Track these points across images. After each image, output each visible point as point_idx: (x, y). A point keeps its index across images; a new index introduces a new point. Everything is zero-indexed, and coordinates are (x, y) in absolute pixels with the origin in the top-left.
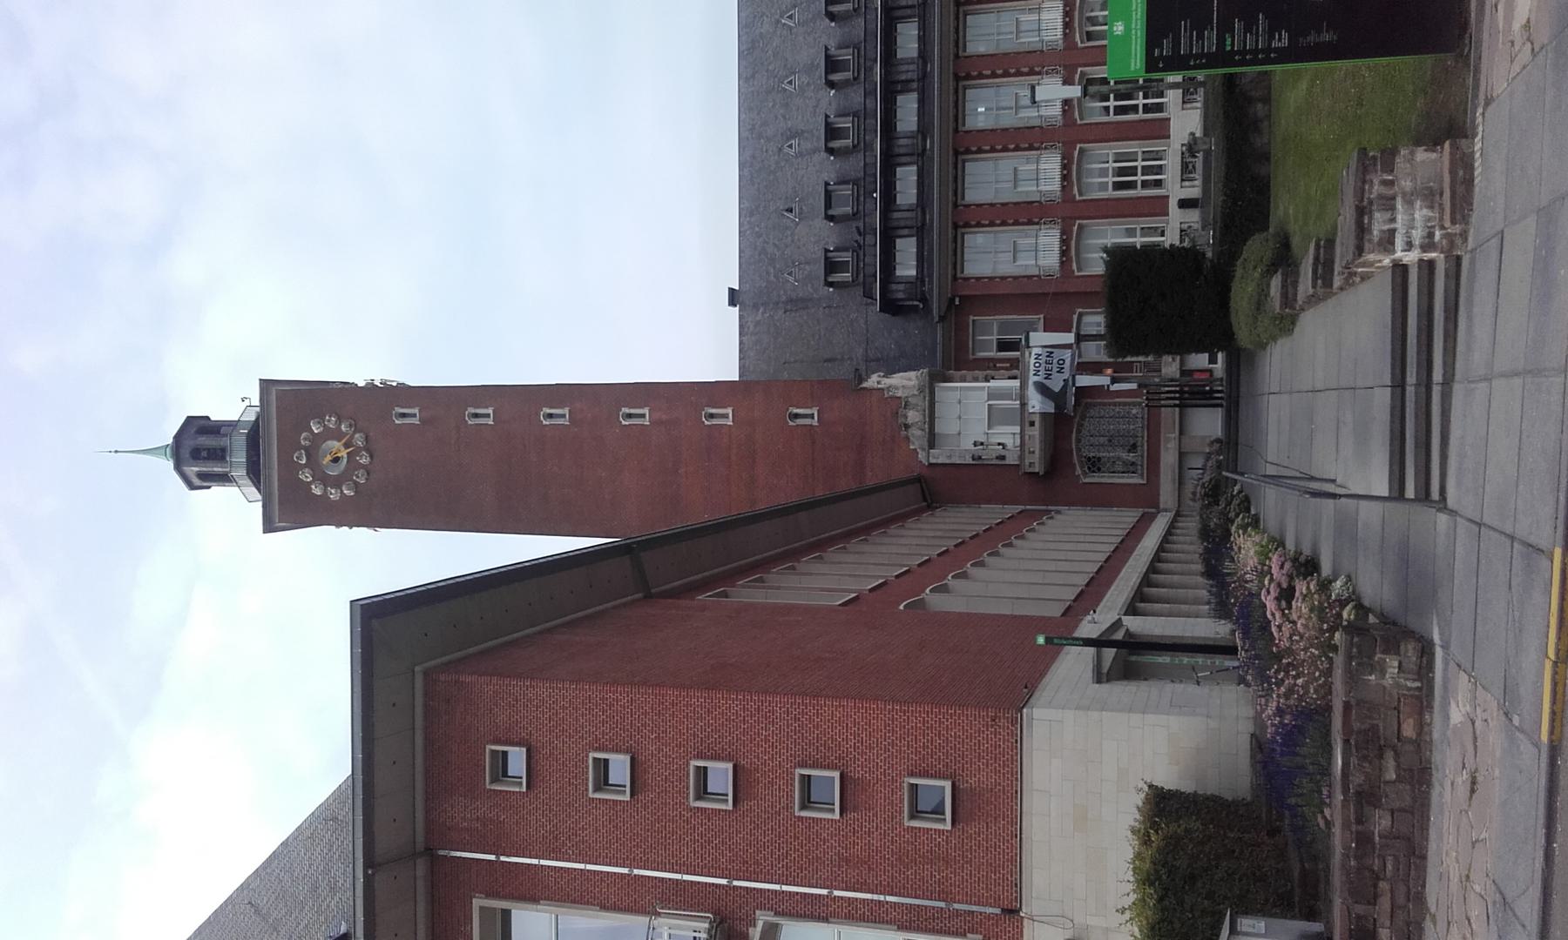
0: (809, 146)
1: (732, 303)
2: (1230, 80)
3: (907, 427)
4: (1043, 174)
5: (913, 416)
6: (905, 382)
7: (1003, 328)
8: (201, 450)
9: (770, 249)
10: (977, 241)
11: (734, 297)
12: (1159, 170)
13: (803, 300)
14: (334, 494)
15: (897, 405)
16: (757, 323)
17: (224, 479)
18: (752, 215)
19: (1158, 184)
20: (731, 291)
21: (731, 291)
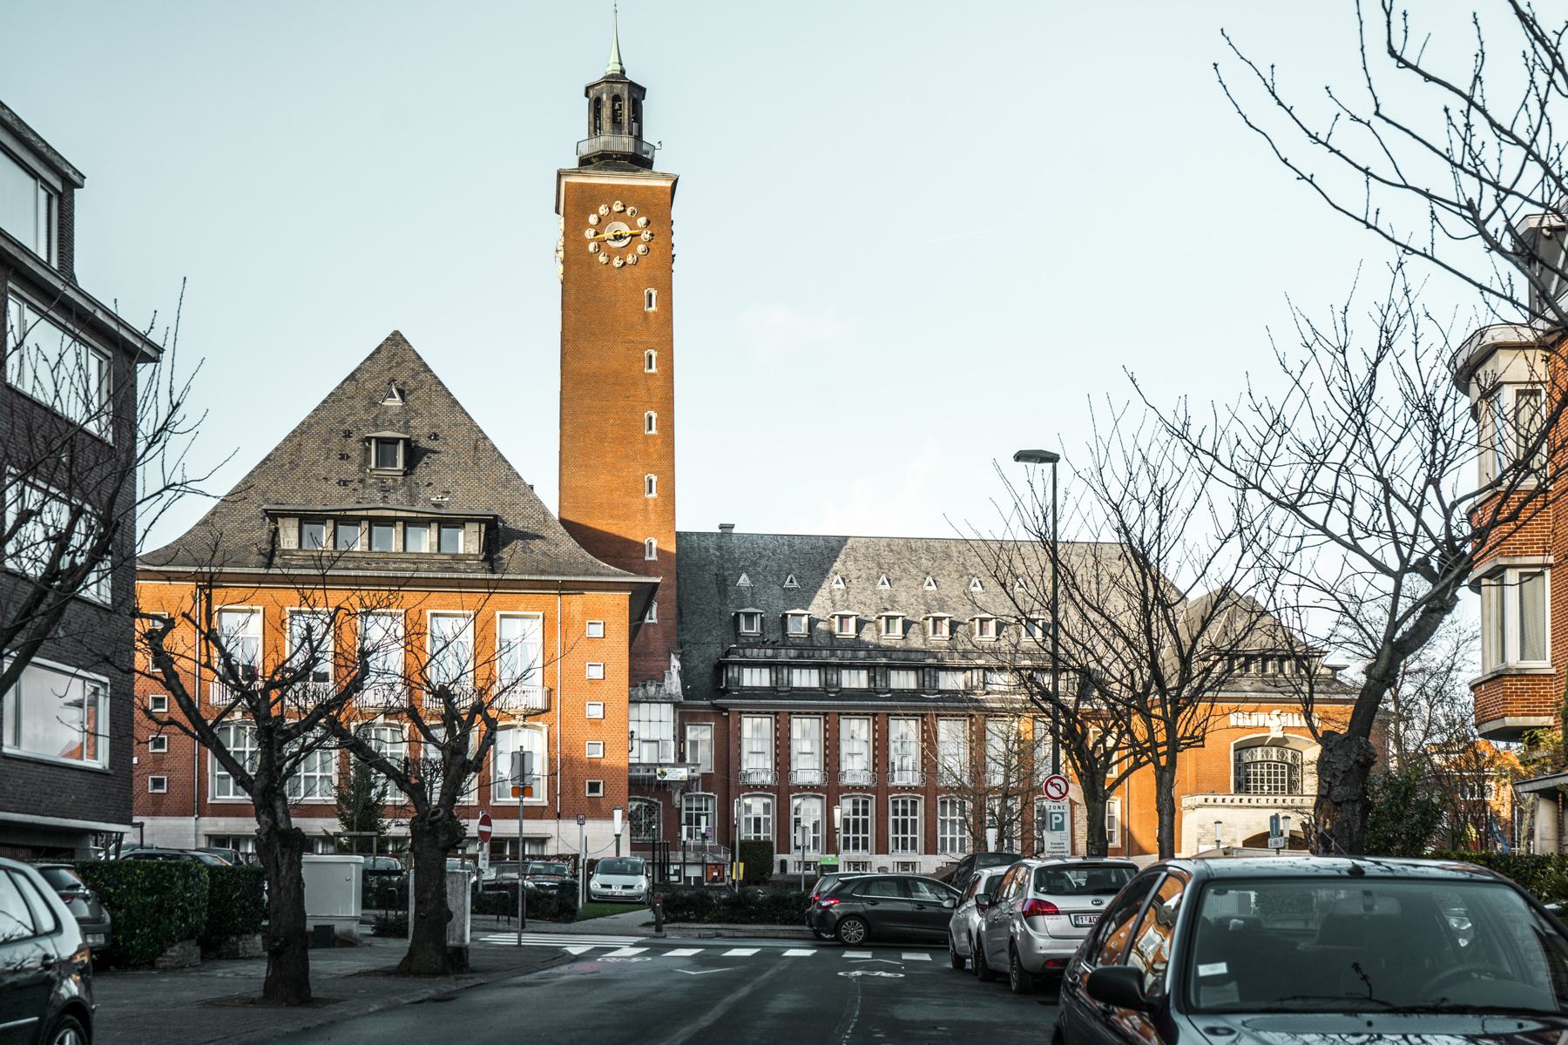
0: (838, 598)
1: (721, 527)
2: (269, 565)
3: (644, 686)
4: (807, 769)
5: (652, 690)
6: (673, 683)
7: (767, 820)
8: (619, 102)
9: (763, 562)
10: (766, 723)
11: (726, 528)
12: (904, 847)
13: (726, 590)
14: (589, 233)
15: (659, 679)
16: (707, 550)
17: (595, 127)
18: (790, 546)
19: (846, 847)
20: (732, 526)
21: (732, 526)
